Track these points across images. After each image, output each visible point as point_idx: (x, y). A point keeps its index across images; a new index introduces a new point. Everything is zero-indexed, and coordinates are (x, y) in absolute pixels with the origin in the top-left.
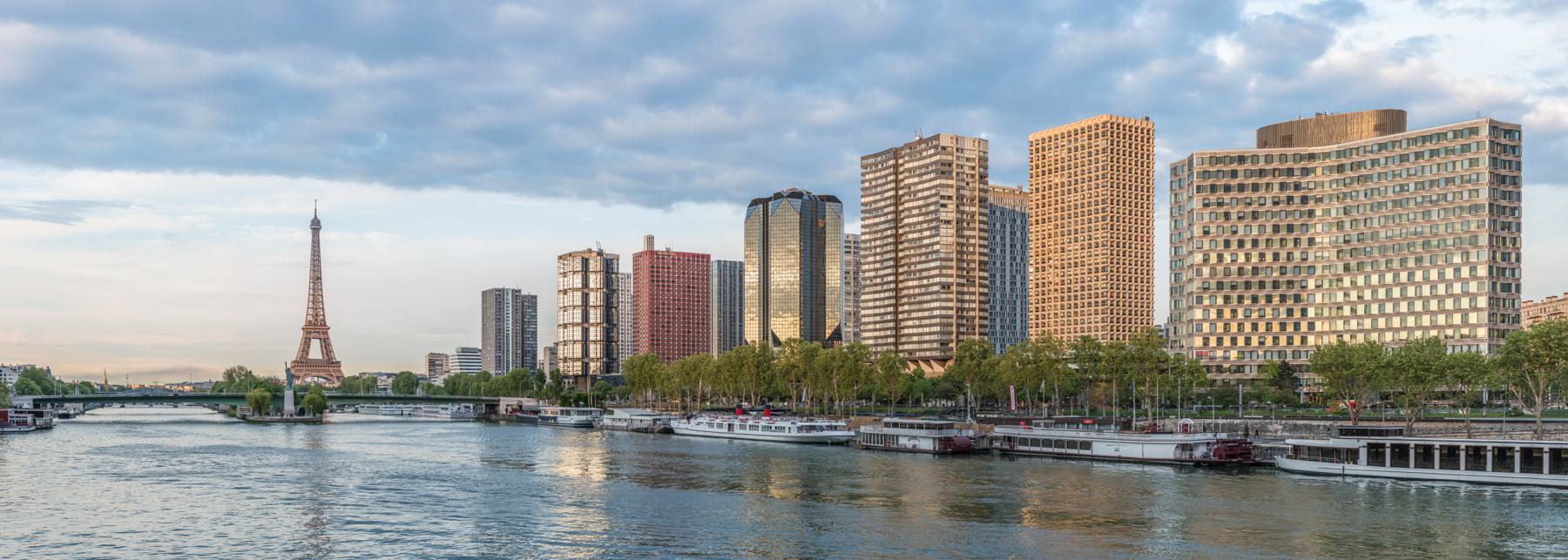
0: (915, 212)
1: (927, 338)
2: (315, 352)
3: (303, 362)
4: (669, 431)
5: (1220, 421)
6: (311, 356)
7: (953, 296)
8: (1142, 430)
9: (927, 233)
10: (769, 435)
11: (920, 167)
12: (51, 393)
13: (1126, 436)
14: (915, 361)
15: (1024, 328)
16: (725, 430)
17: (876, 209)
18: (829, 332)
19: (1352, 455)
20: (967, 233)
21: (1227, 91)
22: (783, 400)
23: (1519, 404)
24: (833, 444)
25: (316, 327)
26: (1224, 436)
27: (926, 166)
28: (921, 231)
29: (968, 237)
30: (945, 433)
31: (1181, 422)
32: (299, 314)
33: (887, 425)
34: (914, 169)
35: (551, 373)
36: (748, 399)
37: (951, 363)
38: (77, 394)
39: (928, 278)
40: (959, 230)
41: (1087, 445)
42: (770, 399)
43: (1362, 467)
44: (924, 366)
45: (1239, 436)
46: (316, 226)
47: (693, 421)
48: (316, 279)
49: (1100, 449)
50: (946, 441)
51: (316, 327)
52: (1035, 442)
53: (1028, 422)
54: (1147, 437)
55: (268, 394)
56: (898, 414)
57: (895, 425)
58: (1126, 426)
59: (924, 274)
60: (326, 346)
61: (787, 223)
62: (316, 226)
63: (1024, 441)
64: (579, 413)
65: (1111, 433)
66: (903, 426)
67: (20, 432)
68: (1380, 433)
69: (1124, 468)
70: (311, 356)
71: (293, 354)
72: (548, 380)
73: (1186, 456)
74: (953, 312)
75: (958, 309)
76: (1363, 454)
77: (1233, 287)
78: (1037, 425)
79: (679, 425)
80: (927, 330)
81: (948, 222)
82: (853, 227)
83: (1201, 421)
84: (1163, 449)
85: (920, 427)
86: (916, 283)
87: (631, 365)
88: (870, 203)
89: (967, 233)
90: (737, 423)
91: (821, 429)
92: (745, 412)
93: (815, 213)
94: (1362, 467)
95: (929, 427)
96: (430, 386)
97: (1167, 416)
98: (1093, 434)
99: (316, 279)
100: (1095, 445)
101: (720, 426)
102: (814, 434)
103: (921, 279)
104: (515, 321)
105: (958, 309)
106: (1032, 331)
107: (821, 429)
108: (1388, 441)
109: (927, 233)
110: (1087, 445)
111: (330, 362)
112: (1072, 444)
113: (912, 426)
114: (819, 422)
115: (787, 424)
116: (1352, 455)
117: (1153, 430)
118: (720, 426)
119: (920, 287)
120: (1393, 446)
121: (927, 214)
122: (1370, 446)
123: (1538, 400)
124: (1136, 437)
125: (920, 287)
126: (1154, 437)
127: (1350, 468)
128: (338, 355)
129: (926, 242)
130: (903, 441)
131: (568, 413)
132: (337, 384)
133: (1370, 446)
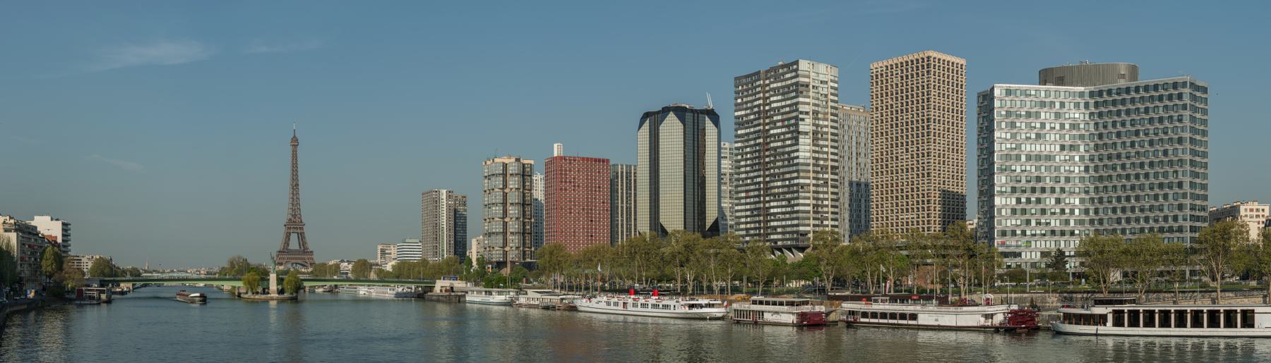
0: (779, 124)
1: (789, 229)
2: (294, 244)
3: (285, 251)
4: (574, 309)
5: (1013, 295)
6: (291, 247)
7: (811, 195)
8: (954, 304)
9: (788, 142)
10: (656, 312)
11: (783, 87)
13: (943, 309)
14: (780, 249)
15: (868, 221)
16: (621, 307)
17: (747, 122)
18: (708, 225)
19: (1102, 320)
20: (821, 143)
22: (669, 281)
23: (1205, 279)
24: (711, 319)
25: (295, 224)
26: (1015, 307)
27: (788, 87)
28: (783, 141)
29: (822, 146)
30: (806, 309)
31: (984, 297)
32: (284, 215)
33: (754, 302)
34: (778, 88)
36: (640, 281)
37: (808, 250)
39: (789, 179)
40: (815, 139)
41: (914, 317)
42: (659, 281)
43: (1109, 328)
44: (787, 253)
45: (1027, 306)
46: (295, 142)
47: (594, 300)
48: (295, 186)
49: (923, 319)
50: (802, 316)
51: (295, 224)
52: (874, 315)
53: (869, 299)
54: (959, 309)
56: (765, 293)
57: (761, 303)
58: (943, 302)
59: (788, 176)
60: (301, 236)
61: (672, 130)
62: (295, 142)
63: (865, 315)
65: (932, 306)
66: (768, 303)
68: (1121, 302)
69: (942, 335)
70: (291, 247)
71: (278, 245)
72: (474, 263)
73: (989, 323)
74: (810, 208)
75: (814, 206)
76: (1110, 317)
77: (1024, 191)
78: (876, 301)
79: (582, 303)
80: (789, 223)
81: (806, 133)
83: (999, 296)
84: (971, 317)
85: (781, 304)
86: (779, 184)
87: (93, 271)
88: (742, 116)
89: (821, 143)
90: (630, 301)
91: (701, 306)
92: (636, 293)
93: (695, 120)
94: (1109, 328)
95: (791, 304)
96: (381, 271)
97: (975, 292)
98: (918, 308)
99: (295, 186)
100: (920, 316)
101: (616, 304)
102: (695, 310)
103: (784, 180)
104: (449, 218)
105: (814, 206)
106: (874, 224)
107: (701, 306)
108: (1126, 308)
109: (788, 142)
110: (914, 317)
112: (903, 316)
113: (774, 304)
114: (703, 301)
115: (672, 303)
116: (1102, 320)
117: (963, 303)
118: (616, 304)
119: (783, 187)
120: (1130, 311)
121: (788, 126)
122: (1115, 312)
123: (1219, 277)
124: (952, 309)
125: (783, 187)
126: (965, 309)
127: (1101, 329)
128: (311, 247)
129: (787, 149)
130: (768, 317)
131: (490, 293)
132: (310, 270)
133: (1115, 312)
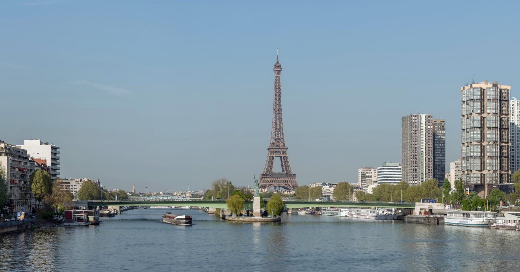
2: (277, 168)
3: (268, 174)
12: (104, 198)
21: (444, 187)
25: (278, 149)
32: (268, 140)
35: (456, 183)
38: (116, 200)
48: (278, 111)
51: (278, 149)
55: (241, 200)
60: (284, 160)
64: (477, 215)
67: (79, 226)
71: (262, 169)
82: (380, 212)
96: (362, 194)
99: (278, 111)
104: (427, 142)
111: (287, 174)
128: (293, 170)
131: (468, 215)
132: (293, 192)
